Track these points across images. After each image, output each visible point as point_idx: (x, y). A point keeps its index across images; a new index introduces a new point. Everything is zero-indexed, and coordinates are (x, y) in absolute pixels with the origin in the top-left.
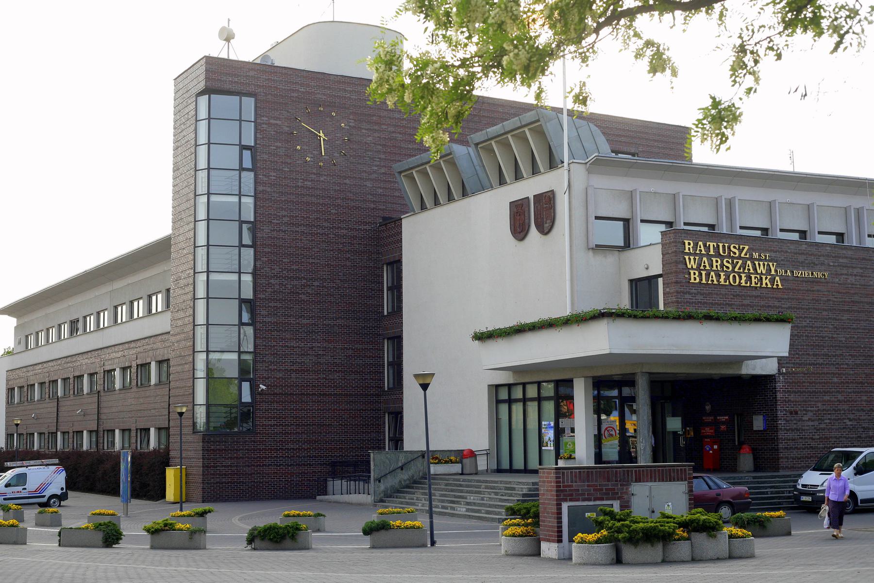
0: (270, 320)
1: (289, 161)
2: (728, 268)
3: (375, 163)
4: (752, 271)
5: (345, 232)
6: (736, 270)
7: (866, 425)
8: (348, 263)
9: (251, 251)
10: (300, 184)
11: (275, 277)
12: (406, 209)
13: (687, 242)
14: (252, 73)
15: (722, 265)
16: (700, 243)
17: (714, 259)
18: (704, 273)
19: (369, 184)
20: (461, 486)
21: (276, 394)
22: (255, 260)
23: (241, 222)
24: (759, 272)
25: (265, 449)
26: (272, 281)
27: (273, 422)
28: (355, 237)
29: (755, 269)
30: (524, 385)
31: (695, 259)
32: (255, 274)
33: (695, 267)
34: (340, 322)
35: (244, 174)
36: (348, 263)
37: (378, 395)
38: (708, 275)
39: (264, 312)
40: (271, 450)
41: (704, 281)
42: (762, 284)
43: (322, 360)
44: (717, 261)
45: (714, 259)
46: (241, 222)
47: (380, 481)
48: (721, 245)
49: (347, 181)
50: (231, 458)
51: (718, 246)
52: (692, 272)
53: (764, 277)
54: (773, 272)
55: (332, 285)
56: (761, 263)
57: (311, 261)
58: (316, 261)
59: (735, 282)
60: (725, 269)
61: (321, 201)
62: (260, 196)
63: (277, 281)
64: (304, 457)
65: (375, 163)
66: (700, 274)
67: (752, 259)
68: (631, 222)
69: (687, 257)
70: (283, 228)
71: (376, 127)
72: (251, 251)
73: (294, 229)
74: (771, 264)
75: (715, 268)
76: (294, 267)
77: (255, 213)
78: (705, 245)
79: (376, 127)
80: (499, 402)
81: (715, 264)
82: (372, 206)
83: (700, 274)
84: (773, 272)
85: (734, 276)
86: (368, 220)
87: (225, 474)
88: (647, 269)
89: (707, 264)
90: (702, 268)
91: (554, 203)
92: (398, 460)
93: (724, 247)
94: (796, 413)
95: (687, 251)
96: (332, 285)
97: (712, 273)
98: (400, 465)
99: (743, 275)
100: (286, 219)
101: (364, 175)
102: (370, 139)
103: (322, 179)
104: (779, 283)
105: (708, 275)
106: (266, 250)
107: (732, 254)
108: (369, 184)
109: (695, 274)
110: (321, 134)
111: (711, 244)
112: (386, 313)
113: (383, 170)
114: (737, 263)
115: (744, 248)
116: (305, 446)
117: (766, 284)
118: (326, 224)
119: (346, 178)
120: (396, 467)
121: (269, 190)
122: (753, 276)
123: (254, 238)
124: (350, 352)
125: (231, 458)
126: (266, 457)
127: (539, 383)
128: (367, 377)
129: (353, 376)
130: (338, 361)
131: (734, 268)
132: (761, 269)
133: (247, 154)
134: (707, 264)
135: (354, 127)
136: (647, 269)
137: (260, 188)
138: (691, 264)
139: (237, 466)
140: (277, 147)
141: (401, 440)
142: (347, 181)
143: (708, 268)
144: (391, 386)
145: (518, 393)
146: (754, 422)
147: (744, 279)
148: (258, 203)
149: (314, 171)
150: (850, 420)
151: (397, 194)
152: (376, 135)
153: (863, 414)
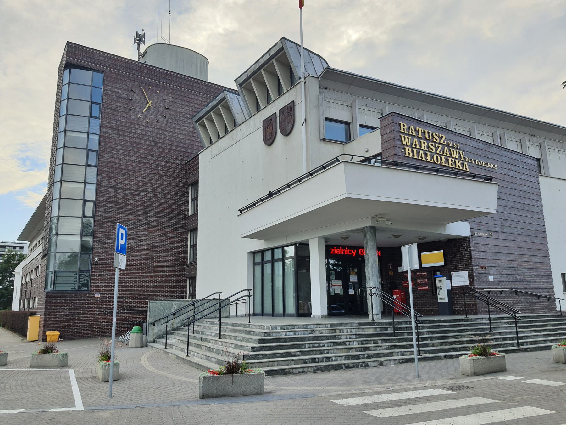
0: (106, 215)
1: (125, 115)
2: (432, 149)
3: (185, 125)
4: (448, 155)
5: (164, 163)
6: (438, 152)
7: (528, 280)
8: (165, 183)
9: (95, 170)
10: (133, 131)
11: (111, 187)
12: (202, 147)
13: (402, 124)
14: (102, 58)
15: (428, 147)
16: (412, 127)
17: (422, 141)
18: (415, 150)
19: (181, 137)
20: (439, 338)
21: (108, 264)
22: (98, 175)
23: (89, 150)
24: (454, 157)
25: (97, 302)
26: (109, 190)
27: (104, 284)
28: (170, 167)
29: (451, 154)
30: (272, 250)
31: (408, 138)
32: (98, 184)
33: (409, 144)
34: (158, 219)
35: (92, 120)
36: (165, 183)
37: (182, 267)
38: (418, 153)
39: (101, 210)
40: (102, 302)
41: (416, 157)
42: (456, 166)
43: (144, 243)
44: (424, 143)
45: (422, 141)
46: (89, 150)
47: (154, 325)
48: (426, 131)
49: (167, 133)
50: (69, 309)
51: (425, 131)
52: (407, 148)
53: (457, 161)
54: (463, 159)
55: (153, 195)
56: (455, 150)
57: (139, 179)
58: (142, 180)
59: (438, 162)
60: (430, 150)
61: (148, 143)
62: (103, 134)
63: (113, 190)
64: (127, 307)
65: (185, 125)
66: (413, 151)
67: (448, 146)
68: (351, 125)
69: (403, 136)
70: (119, 157)
71: (187, 104)
72: (95, 170)
73: (127, 158)
74: (461, 152)
75: (423, 148)
76: (127, 182)
77: (100, 145)
78: (415, 130)
79: (187, 104)
80: (254, 264)
81: (423, 145)
82: (183, 150)
83: (413, 151)
84: (463, 159)
85: (437, 156)
86: (180, 158)
87: (63, 321)
88: (367, 152)
89: (417, 144)
90: (414, 146)
91: (294, 110)
92: (171, 308)
93: (429, 133)
94: (485, 268)
95: (402, 131)
96: (153, 195)
97: (421, 152)
98: (173, 311)
99: (443, 157)
100: (121, 151)
101: (178, 131)
102: (183, 110)
103: (149, 129)
104: (467, 167)
105: (418, 153)
106: (106, 169)
107: (435, 140)
108: (181, 137)
109: (409, 150)
110: (150, 103)
111: (420, 129)
112: (190, 215)
113: (191, 129)
114: (439, 147)
115: (442, 137)
116: (129, 300)
117: (459, 167)
118: (150, 157)
119: (166, 131)
120: (169, 312)
121: (110, 131)
122: (450, 159)
123: (98, 161)
124: (164, 239)
125: (69, 309)
126: (97, 308)
127: (282, 247)
128: (176, 254)
129: (166, 254)
130: (155, 244)
131: (436, 150)
132: (455, 155)
133: (96, 108)
134: (417, 144)
135: (172, 101)
136: (367, 152)
137: (104, 130)
138: (406, 141)
139: (73, 314)
140: (117, 106)
141: (195, 296)
142: (167, 133)
143: (418, 147)
144: (192, 260)
145: (268, 256)
146: (460, 273)
147: (444, 160)
148: (102, 139)
149: (144, 124)
150: (519, 275)
151: (199, 144)
152: (187, 108)
153: (526, 271)
